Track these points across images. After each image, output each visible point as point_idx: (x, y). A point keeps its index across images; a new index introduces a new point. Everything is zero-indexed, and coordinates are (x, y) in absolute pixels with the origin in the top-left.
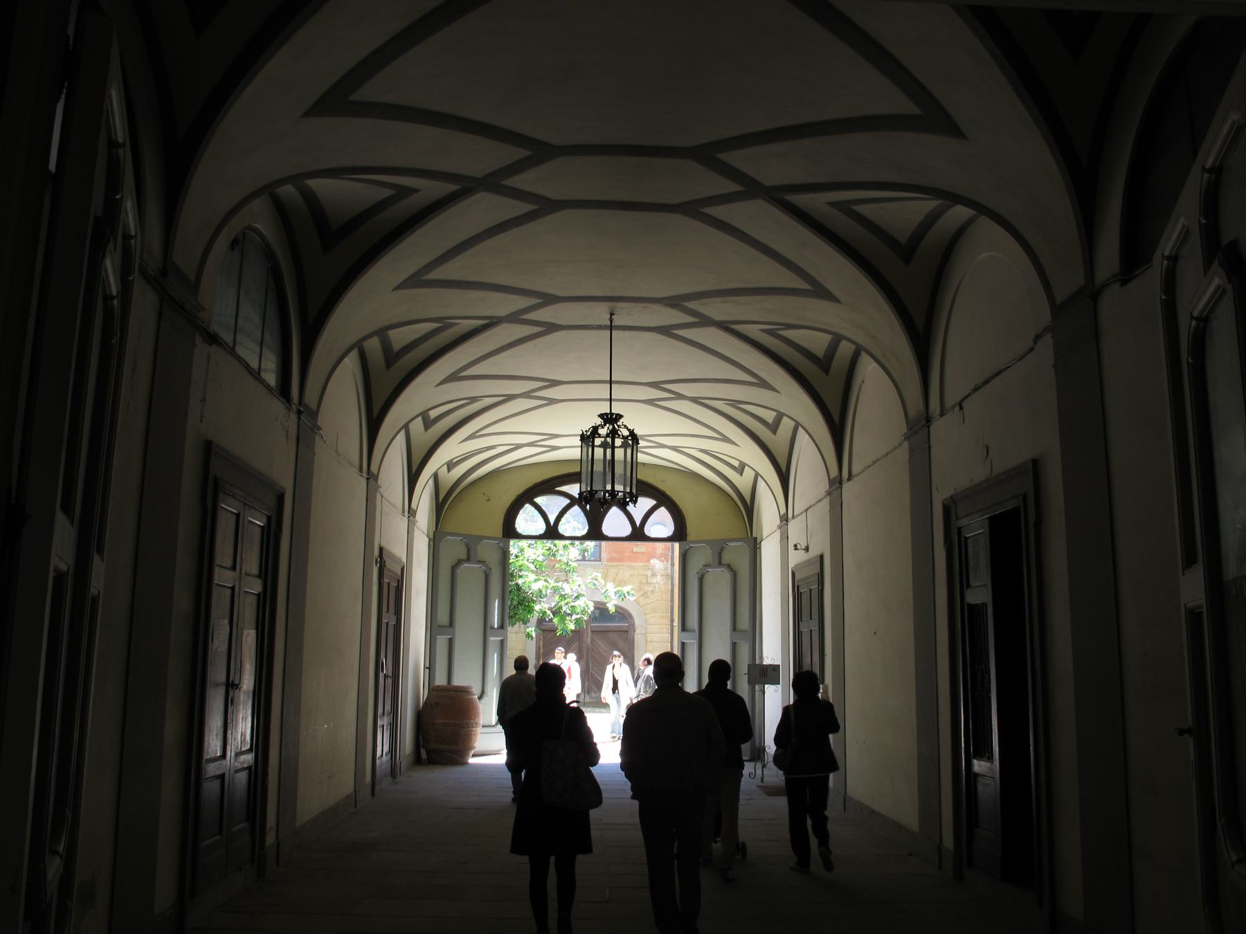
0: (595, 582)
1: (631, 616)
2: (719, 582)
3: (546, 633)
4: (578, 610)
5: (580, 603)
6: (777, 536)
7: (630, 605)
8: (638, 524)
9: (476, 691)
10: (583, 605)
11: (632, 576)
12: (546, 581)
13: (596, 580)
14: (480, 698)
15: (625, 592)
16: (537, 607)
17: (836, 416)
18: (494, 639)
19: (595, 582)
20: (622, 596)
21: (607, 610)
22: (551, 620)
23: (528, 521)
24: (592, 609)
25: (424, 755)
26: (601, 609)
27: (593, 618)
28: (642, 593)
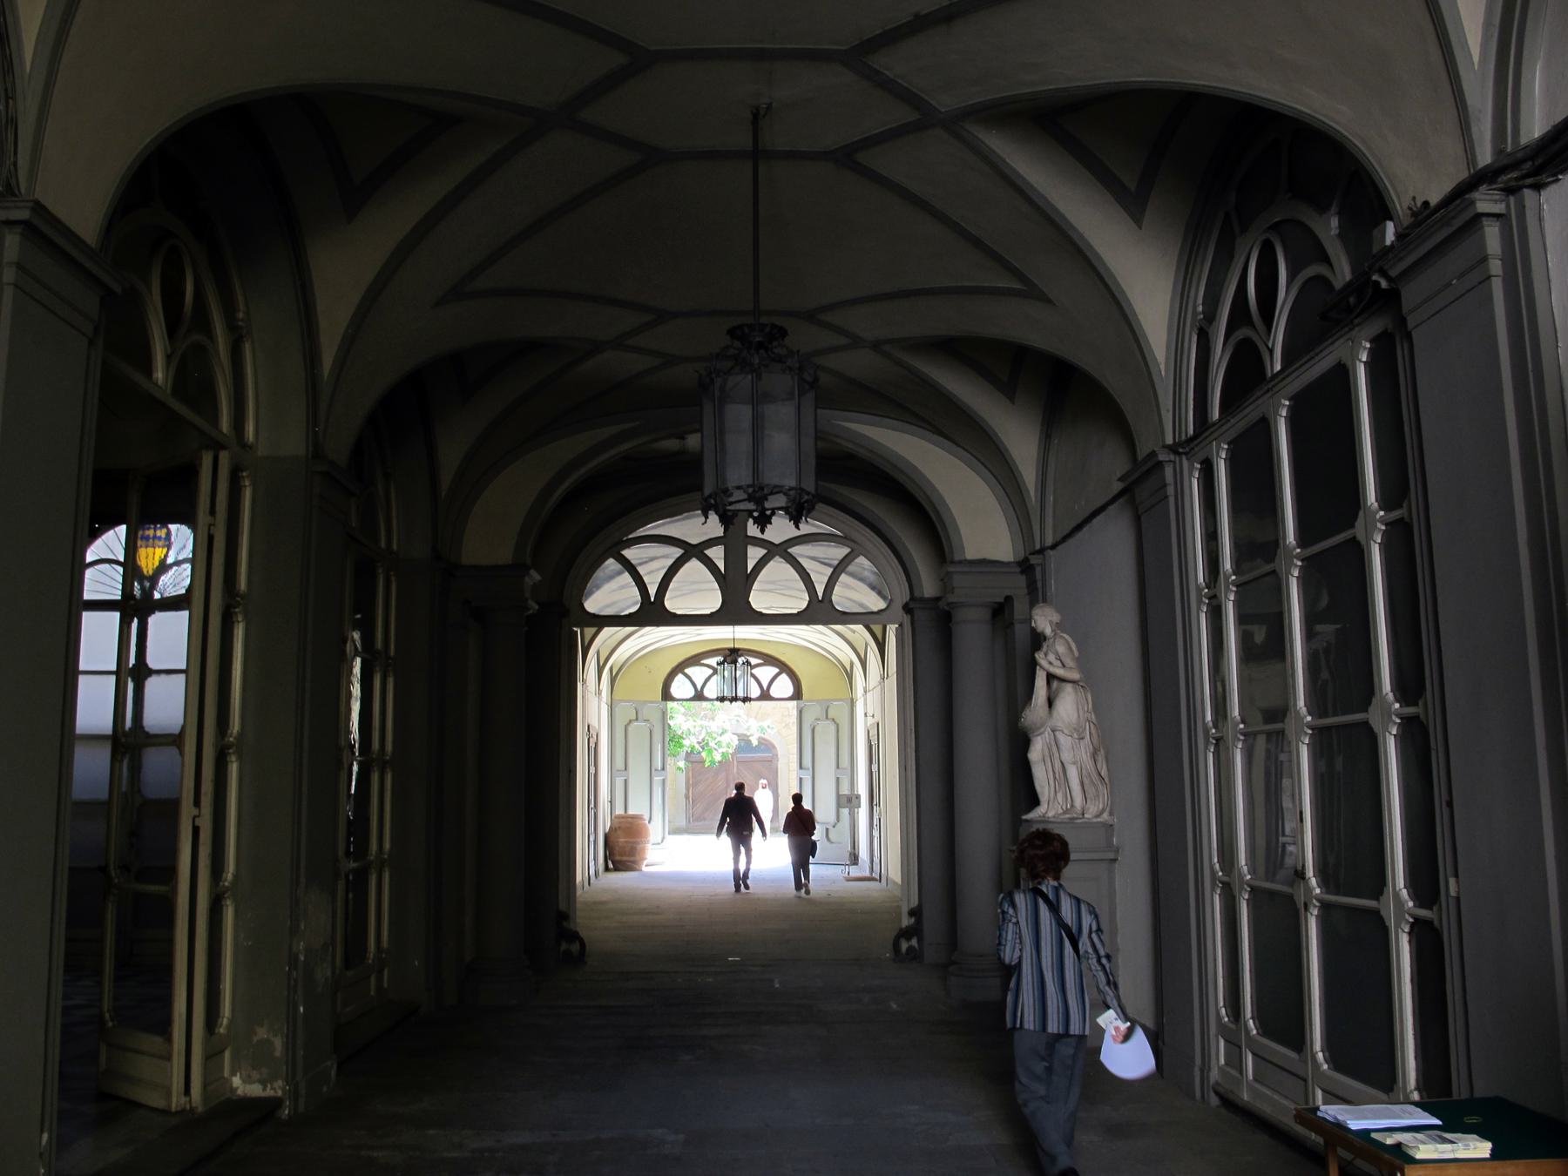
0: (739, 719)
1: (774, 747)
2: (826, 733)
3: (695, 764)
4: (724, 744)
5: (725, 739)
6: (862, 699)
7: (771, 736)
8: (765, 688)
9: (646, 817)
10: (728, 740)
11: (774, 708)
12: (695, 721)
13: (739, 716)
14: (649, 822)
15: (766, 727)
16: (686, 742)
17: (880, 637)
18: (657, 779)
19: (738, 718)
20: (762, 730)
21: (749, 742)
22: (700, 753)
23: (681, 687)
24: (737, 742)
25: (611, 866)
26: (744, 742)
27: (739, 749)
28: (784, 725)
